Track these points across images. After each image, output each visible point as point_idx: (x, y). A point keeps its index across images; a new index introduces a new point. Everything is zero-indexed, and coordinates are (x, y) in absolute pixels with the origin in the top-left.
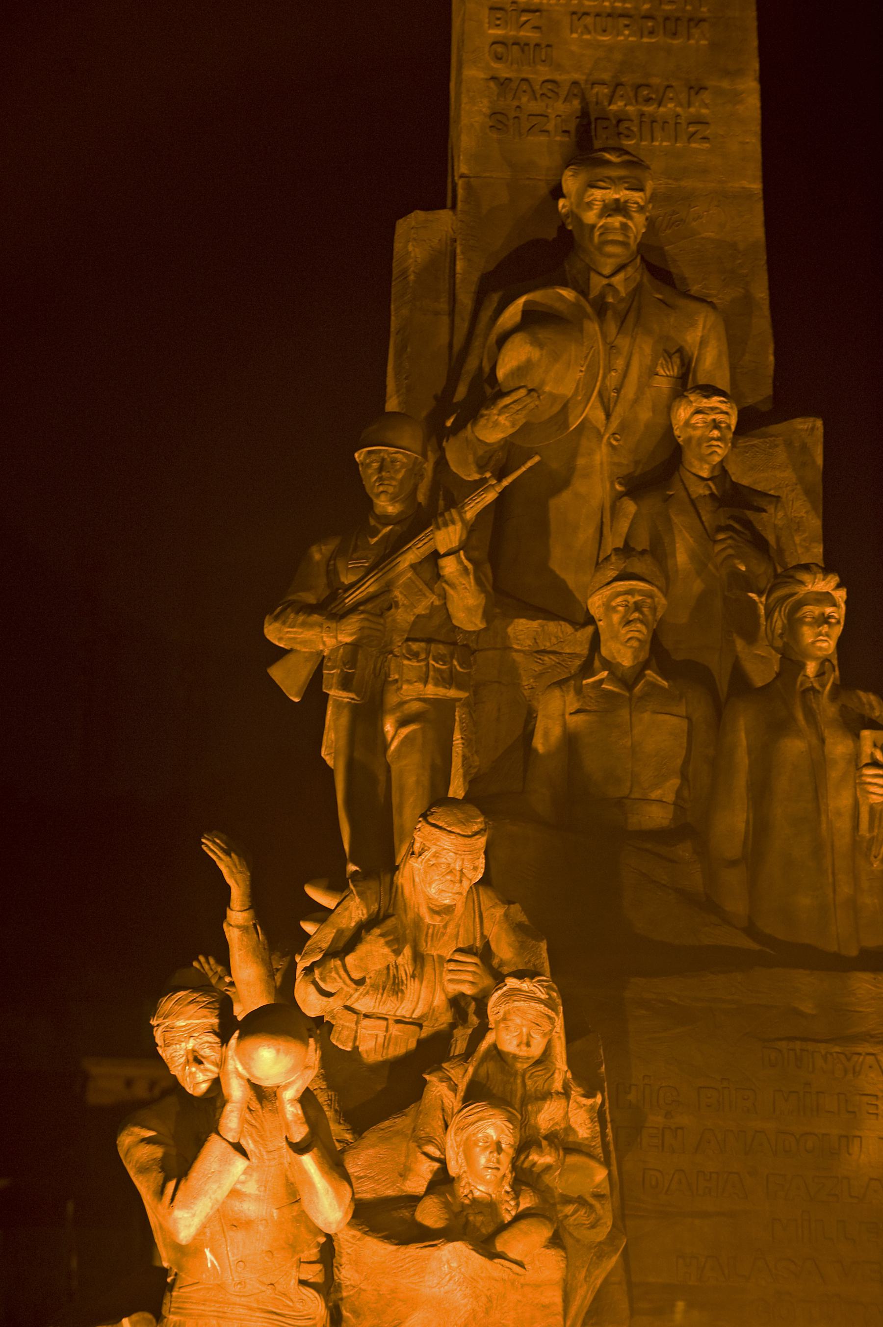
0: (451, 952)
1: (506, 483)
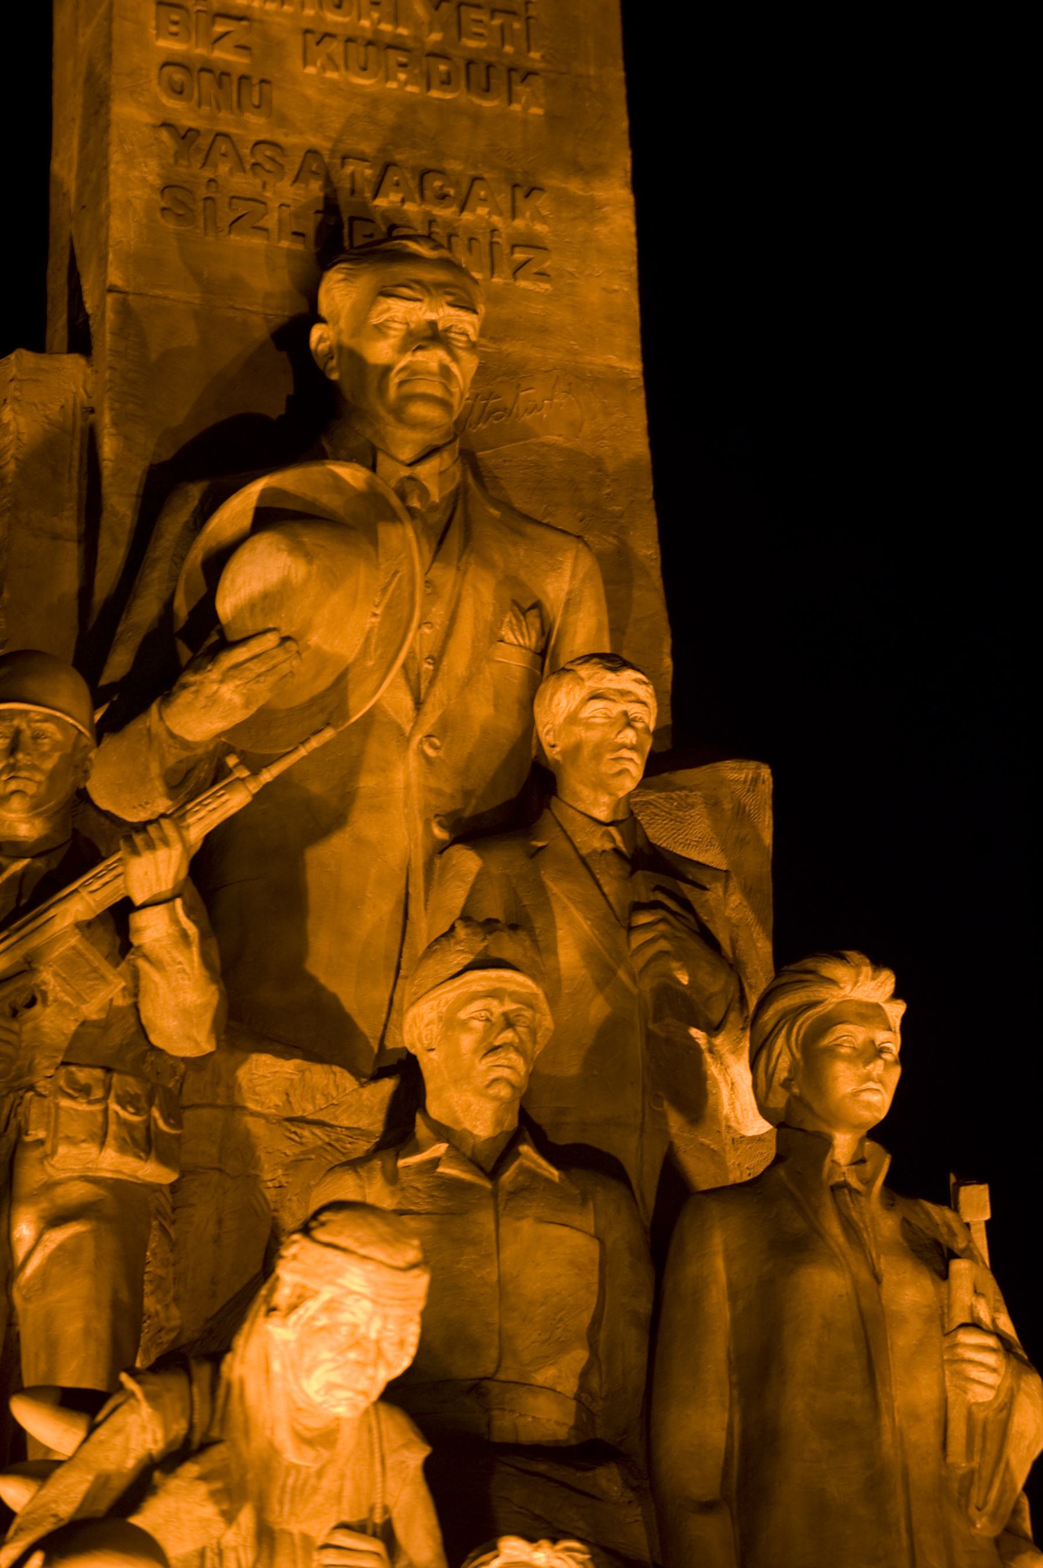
1: (267, 776)
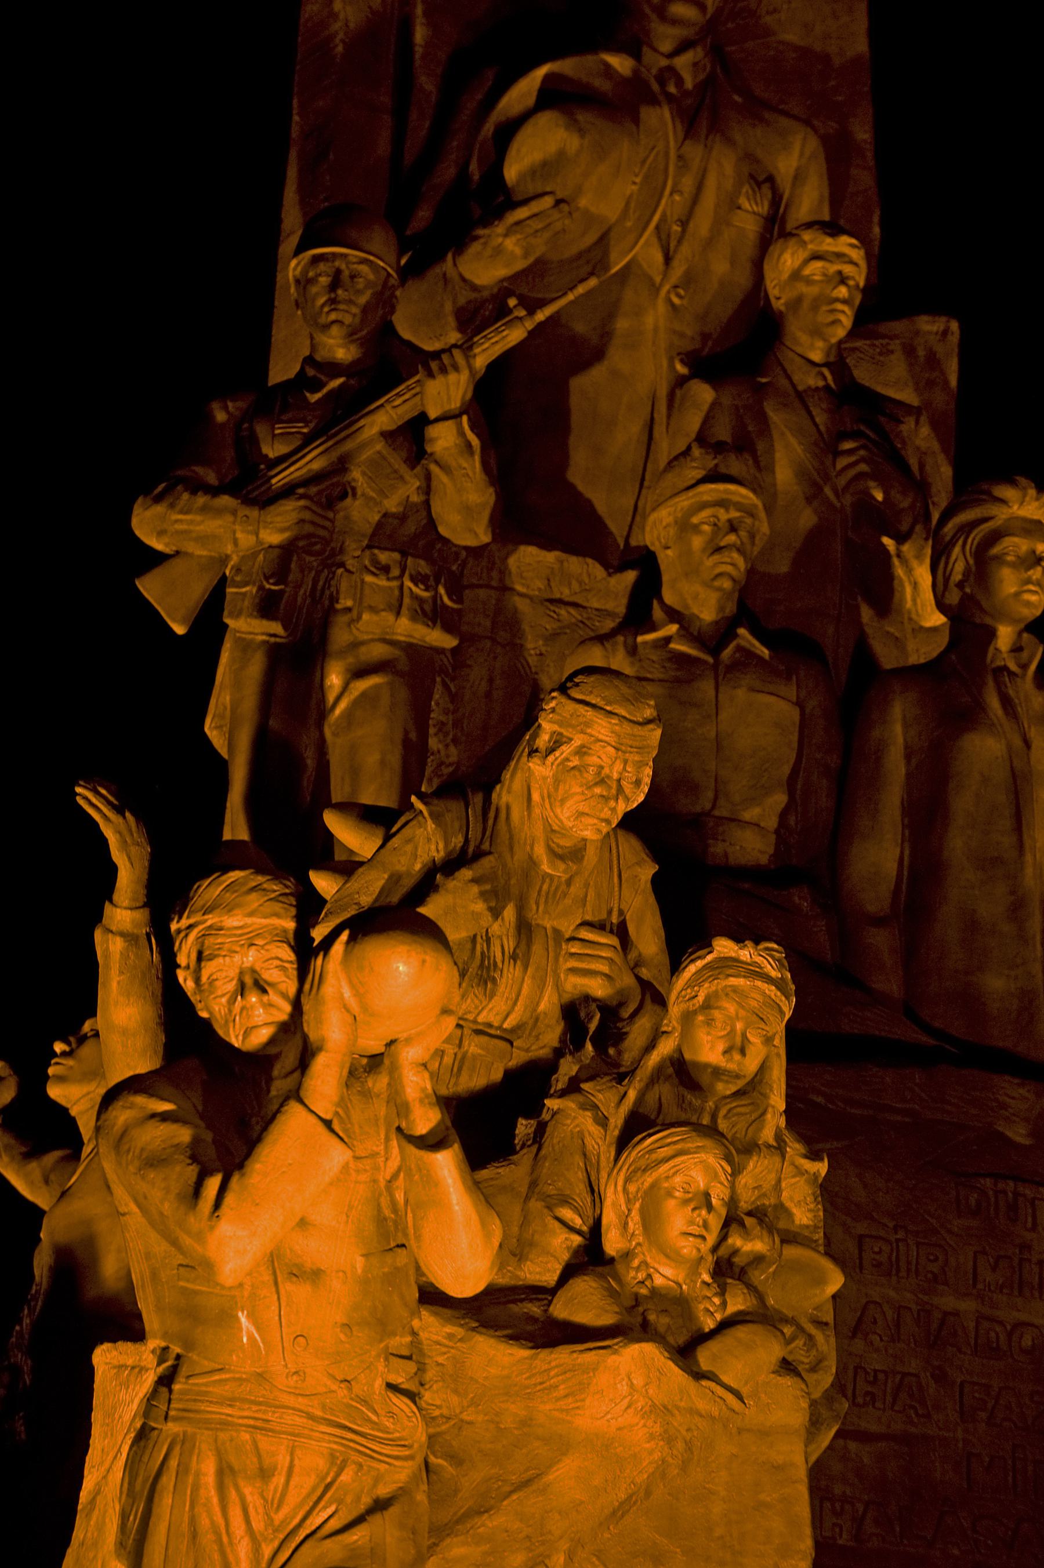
0: (572, 928)
1: (541, 316)
